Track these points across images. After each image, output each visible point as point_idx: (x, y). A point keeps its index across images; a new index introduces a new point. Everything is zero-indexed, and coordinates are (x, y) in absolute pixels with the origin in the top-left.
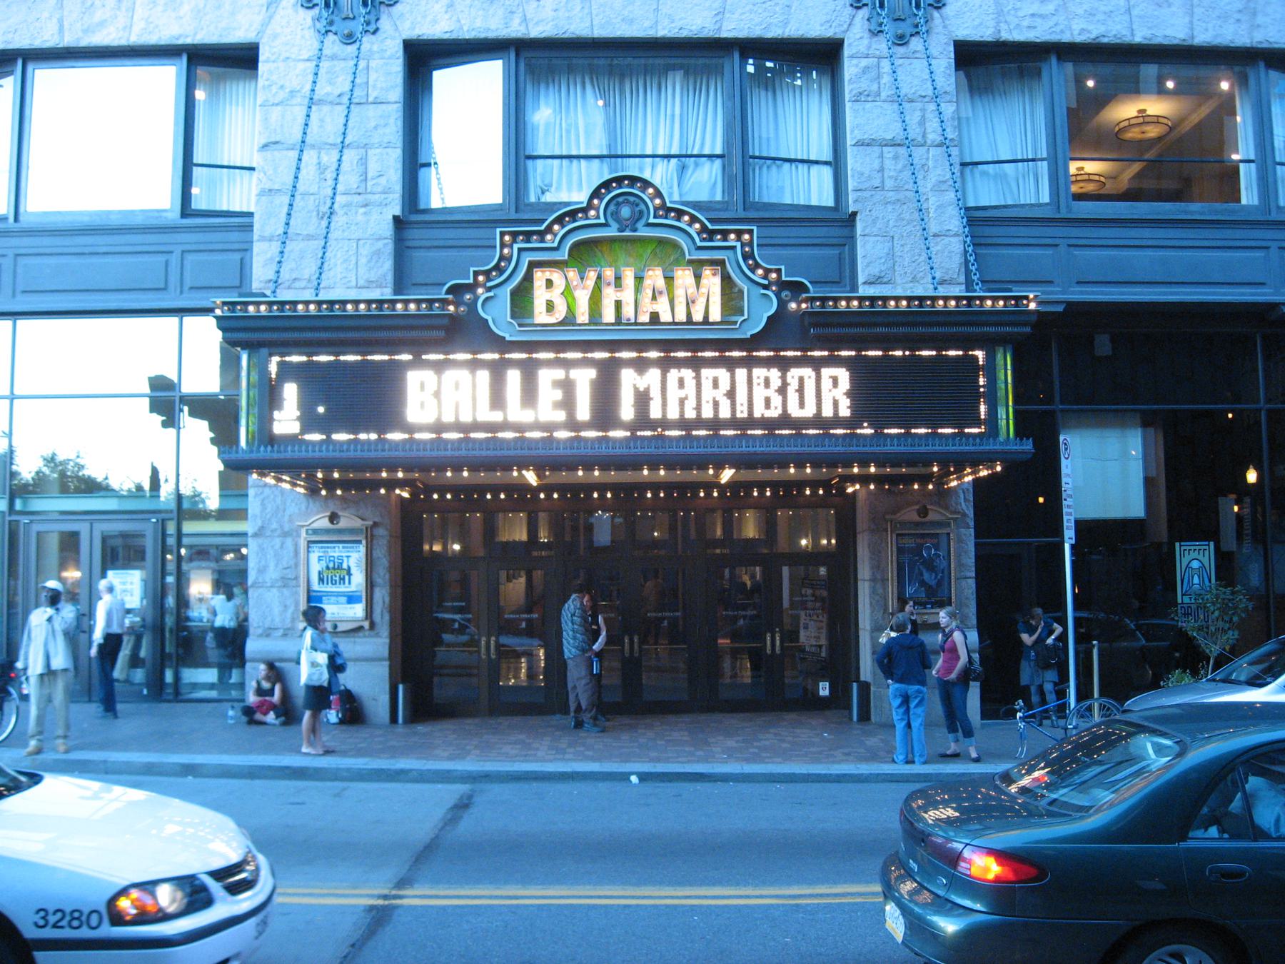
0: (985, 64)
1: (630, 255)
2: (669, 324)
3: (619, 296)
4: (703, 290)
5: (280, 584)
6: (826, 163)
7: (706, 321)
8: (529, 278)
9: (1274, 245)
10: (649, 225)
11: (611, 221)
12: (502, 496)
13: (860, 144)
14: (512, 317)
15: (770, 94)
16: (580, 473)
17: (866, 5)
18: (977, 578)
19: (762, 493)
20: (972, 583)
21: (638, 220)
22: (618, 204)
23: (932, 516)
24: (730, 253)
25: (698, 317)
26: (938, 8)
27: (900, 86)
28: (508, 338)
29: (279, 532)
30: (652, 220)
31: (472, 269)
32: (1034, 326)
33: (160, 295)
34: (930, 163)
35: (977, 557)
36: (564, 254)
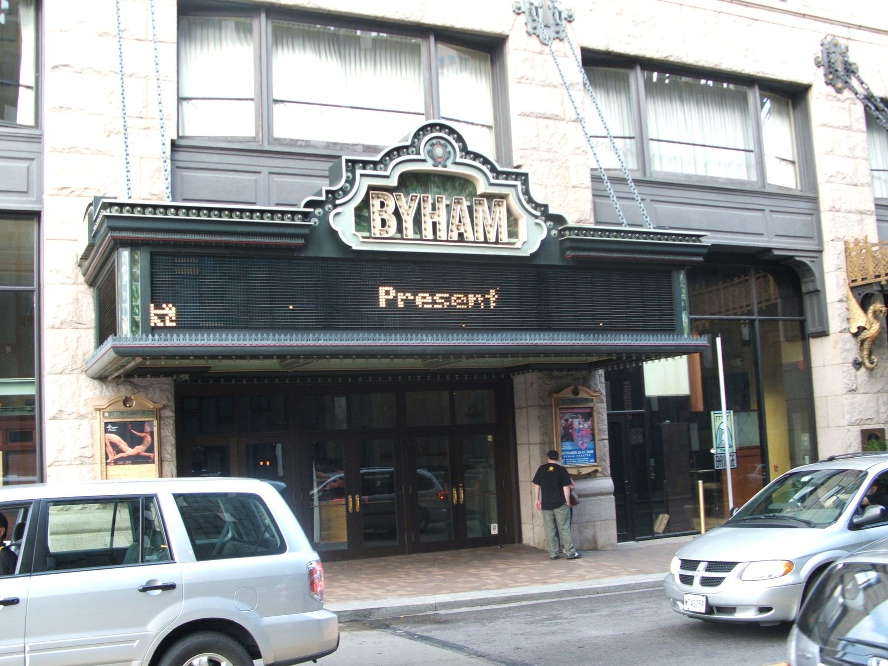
0: (604, 66)
1: (445, 190)
2: (447, 241)
3: (436, 219)
5: (78, 462)
9: (768, 209)
11: (428, 159)
13: (523, 115)
15: (417, 71)
17: (523, 12)
18: (609, 440)
20: (606, 443)
21: (448, 158)
22: (433, 145)
23: (582, 395)
24: (513, 189)
25: (492, 237)
26: (570, 22)
27: (543, 74)
28: (354, 248)
29: (75, 415)
30: (458, 160)
32: (705, 256)
33: (23, 198)
35: (609, 423)
36: (394, 182)
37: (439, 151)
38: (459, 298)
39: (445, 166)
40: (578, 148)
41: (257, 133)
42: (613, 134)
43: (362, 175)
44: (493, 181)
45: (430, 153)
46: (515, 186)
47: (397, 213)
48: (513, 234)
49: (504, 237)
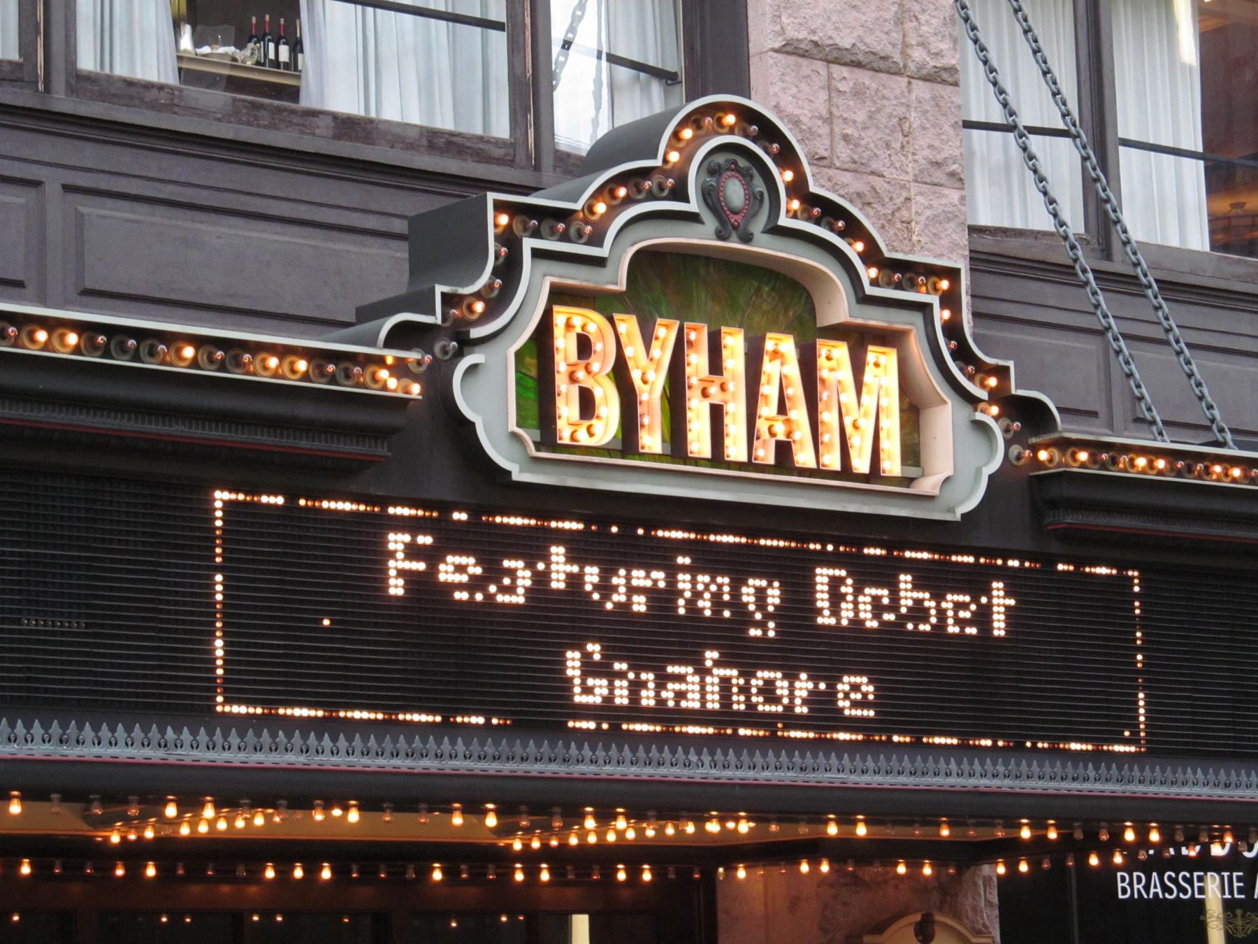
2: (739, 466)
4: (869, 400)
6: (1127, 143)
7: (875, 472)
8: (544, 330)
10: (776, 230)
11: (707, 216)
12: (151, 872)
13: (791, 49)
14: (519, 425)
16: (457, 820)
19: (634, 873)
21: (755, 215)
25: (861, 464)
28: (517, 477)
30: (784, 221)
31: (1011, 364)
34: (914, 118)
36: (617, 279)
37: (735, 192)
38: (855, 688)
39: (747, 238)
40: (937, 164)
41: (26, 47)
42: (1025, 120)
43: (537, 254)
44: (870, 290)
45: (711, 197)
46: (925, 308)
47: (621, 374)
48: (912, 453)
49: (892, 465)
